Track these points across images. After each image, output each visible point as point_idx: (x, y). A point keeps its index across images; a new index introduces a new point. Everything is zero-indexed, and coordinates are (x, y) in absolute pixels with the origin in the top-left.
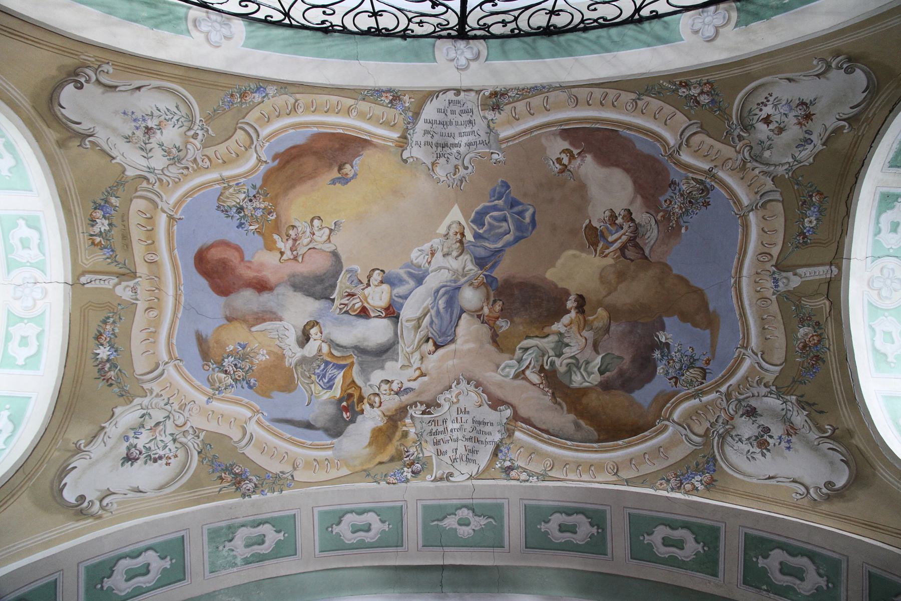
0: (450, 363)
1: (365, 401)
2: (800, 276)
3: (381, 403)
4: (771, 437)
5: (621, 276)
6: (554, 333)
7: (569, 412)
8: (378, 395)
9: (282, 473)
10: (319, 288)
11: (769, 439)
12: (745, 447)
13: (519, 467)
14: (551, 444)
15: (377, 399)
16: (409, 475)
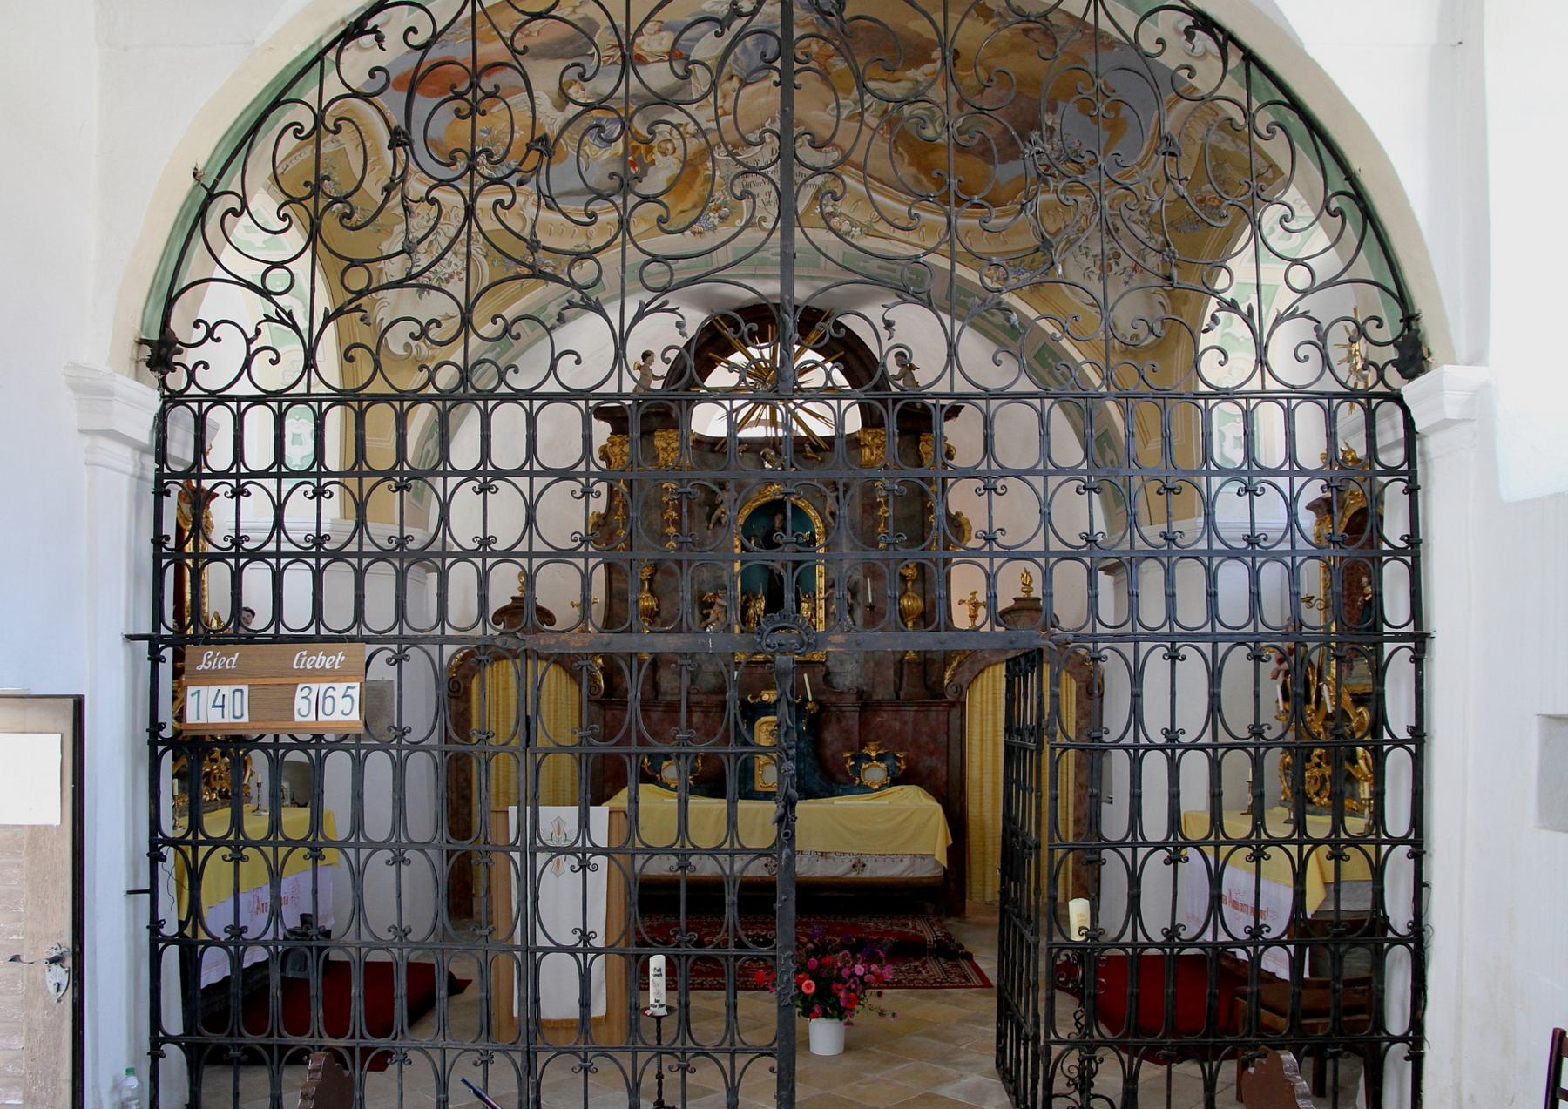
0: (763, 100)
1: (655, 150)
2: (1238, 147)
3: (675, 149)
4: (1117, 264)
5: (1015, 47)
6: (908, 80)
7: (911, 164)
8: (670, 141)
9: (578, 246)
10: (570, 48)
11: (1113, 265)
12: (1088, 262)
13: (841, 214)
14: (882, 194)
15: (669, 146)
16: (716, 221)
